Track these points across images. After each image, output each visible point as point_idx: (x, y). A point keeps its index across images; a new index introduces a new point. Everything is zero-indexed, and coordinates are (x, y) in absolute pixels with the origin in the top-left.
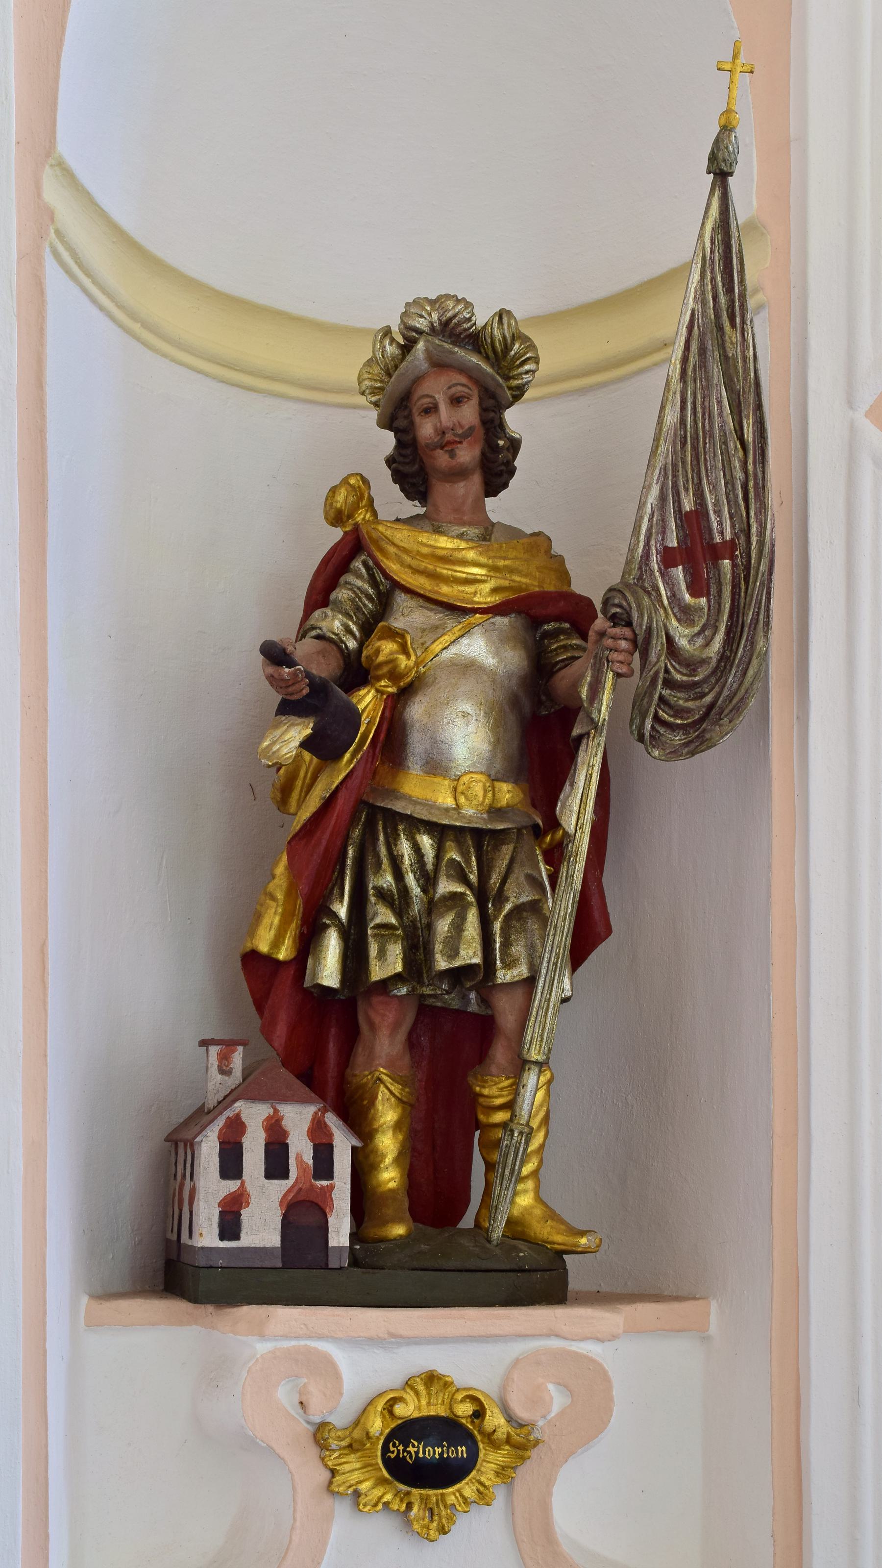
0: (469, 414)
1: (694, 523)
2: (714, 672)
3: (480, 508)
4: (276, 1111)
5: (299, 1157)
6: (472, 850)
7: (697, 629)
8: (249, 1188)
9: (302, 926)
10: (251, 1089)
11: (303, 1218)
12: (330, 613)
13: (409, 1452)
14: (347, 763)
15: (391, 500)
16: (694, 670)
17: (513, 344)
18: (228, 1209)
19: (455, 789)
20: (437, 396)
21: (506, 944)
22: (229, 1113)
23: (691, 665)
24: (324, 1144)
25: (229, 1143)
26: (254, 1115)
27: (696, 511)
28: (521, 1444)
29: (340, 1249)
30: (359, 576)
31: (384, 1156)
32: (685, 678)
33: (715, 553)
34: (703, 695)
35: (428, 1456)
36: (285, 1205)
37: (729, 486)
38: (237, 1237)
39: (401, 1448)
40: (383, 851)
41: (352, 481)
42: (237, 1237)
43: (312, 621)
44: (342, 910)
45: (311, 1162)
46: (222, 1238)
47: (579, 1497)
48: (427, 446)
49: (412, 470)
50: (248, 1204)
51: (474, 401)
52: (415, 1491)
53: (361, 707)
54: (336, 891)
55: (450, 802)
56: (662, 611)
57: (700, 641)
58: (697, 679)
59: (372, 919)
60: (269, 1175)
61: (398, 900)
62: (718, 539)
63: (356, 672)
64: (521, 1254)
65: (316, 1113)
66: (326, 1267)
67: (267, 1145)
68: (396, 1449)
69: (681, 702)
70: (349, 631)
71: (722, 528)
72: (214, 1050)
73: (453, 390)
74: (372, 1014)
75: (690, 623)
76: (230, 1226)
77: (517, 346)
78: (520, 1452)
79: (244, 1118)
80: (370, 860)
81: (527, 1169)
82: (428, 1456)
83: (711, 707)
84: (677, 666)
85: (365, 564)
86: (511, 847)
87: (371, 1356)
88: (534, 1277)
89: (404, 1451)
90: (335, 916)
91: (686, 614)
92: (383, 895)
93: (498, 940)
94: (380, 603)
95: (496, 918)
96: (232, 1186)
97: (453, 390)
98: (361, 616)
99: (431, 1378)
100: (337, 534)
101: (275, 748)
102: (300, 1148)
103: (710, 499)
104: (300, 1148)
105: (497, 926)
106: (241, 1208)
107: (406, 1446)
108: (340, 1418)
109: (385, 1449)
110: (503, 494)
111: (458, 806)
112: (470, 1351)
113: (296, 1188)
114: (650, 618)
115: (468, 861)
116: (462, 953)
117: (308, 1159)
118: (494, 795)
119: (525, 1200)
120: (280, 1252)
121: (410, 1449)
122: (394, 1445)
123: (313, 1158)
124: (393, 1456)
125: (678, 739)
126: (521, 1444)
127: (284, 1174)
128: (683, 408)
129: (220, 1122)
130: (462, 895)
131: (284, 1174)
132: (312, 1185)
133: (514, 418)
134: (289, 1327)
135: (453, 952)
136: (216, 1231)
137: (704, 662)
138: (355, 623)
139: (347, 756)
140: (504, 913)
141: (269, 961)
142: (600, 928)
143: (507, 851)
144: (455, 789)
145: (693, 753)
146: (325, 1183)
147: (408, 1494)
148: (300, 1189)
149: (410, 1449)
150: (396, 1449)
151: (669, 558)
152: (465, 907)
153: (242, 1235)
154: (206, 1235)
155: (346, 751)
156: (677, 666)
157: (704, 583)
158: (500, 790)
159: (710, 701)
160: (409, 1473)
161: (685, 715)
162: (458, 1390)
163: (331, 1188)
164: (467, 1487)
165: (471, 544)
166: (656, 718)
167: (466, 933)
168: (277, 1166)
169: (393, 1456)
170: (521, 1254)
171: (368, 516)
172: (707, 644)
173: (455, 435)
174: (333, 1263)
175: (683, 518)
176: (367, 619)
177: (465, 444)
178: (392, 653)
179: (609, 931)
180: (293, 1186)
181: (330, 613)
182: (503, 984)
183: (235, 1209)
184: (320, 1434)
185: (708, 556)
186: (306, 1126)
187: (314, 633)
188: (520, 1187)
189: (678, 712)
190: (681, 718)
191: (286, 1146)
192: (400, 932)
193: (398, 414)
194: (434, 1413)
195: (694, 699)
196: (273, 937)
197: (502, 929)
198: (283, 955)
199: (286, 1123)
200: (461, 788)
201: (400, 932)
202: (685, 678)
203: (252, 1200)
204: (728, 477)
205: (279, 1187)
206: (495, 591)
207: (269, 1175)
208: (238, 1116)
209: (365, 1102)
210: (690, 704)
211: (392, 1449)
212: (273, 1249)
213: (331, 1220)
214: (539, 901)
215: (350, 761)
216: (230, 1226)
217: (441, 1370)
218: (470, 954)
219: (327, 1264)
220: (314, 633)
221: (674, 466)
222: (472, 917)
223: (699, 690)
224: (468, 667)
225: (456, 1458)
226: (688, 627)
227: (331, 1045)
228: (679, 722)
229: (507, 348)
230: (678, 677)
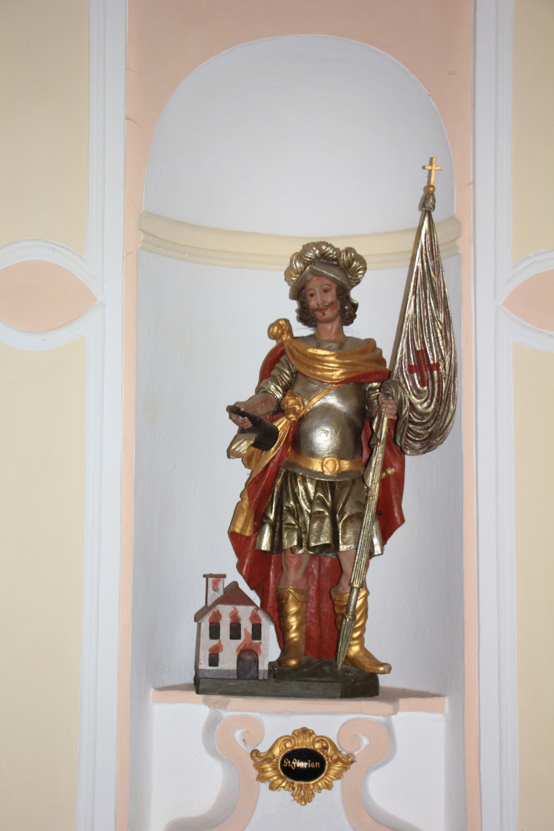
0: (330, 297)
1: (421, 355)
2: (432, 418)
3: (340, 331)
4: (235, 609)
5: (246, 630)
6: (329, 491)
7: (423, 400)
8: (222, 643)
9: (254, 522)
10: (222, 600)
11: (248, 656)
12: (270, 382)
13: (293, 764)
14: (273, 452)
15: (301, 330)
16: (423, 417)
17: (353, 263)
18: (213, 652)
19: (322, 463)
20: (316, 290)
21: (344, 533)
22: (214, 610)
23: (422, 415)
24: (257, 624)
25: (214, 623)
26: (225, 610)
27: (422, 350)
28: (347, 762)
29: (264, 671)
30: (283, 365)
31: (292, 627)
32: (419, 421)
33: (431, 368)
34: (428, 428)
35: (304, 766)
36: (239, 651)
37: (436, 340)
38: (217, 665)
39: (289, 762)
40: (290, 491)
41: (281, 322)
42: (217, 665)
43: (262, 385)
44: (272, 517)
45: (251, 632)
46: (210, 665)
47: (382, 788)
48: (313, 310)
49: (306, 316)
50: (222, 650)
51: (334, 291)
52: (296, 783)
53: (279, 428)
54: (270, 507)
55: (319, 470)
56: (408, 392)
57: (425, 405)
58: (424, 421)
59: (285, 521)
60: (232, 638)
61: (297, 512)
62: (432, 362)
63: (280, 410)
64: (350, 675)
65: (253, 610)
66: (257, 678)
67: (231, 624)
68: (287, 763)
69: (418, 431)
70: (278, 390)
71: (432, 358)
72: (211, 580)
73: (323, 287)
74: (287, 562)
75: (420, 398)
76: (214, 660)
77: (355, 263)
78: (345, 766)
79: (221, 612)
80: (285, 494)
81: (356, 635)
82: (304, 766)
83: (431, 433)
84: (416, 415)
85: (285, 360)
86: (348, 489)
87: (279, 721)
88: (362, 683)
89: (291, 763)
90: (269, 519)
91: (419, 394)
92: (290, 510)
93: (340, 531)
94: (293, 377)
95: (340, 522)
96: (215, 642)
97: (323, 287)
98: (284, 383)
99: (305, 731)
100: (273, 344)
101: (238, 449)
102: (246, 626)
103: (428, 346)
104: (246, 626)
105: (340, 525)
106: (219, 652)
107: (291, 761)
108: (263, 748)
109: (282, 762)
110: (355, 321)
111: (323, 472)
112: (326, 719)
113: (244, 644)
114: (401, 396)
115: (327, 497)
116: (322, 539)
117: (250, 630)
118: (340, 466)
119: (355, 649)
120: (236, 672)
121: (293, 763)
122: (286, 761)
123: (252, 630)
124: (285, 766)
125: (418, 446)
126: (347, 762)
127: (239, 637)
128: (415, 307)
129: (210, 614)
130: (323, 512)
131: (239, 637)
132: (251, 643)
133: (355, 294)
134: (238, 708)
135: (318, 540)
136: (208, 662)
137: (428, 414)
138: (280, 386)
139: (273, 449)
140: (344, 519)
141: (240, 536)
142: (399, 521)
143: (346, 491)
144: (322, 463)
145: (424, 453)
146: (257, 641)
147: (293, 783)
148: (246, 644)
149: (293, 763)
150: (287, 763)
151: (411, 370)
152: (324, 517)
153: (220, 664)
154: (204, 665)
155: (272, 446)
156: (416, 415)
157: (426, 380)
158: (343, 464)
159: (433, 430)
160: (292, 774)
161: (421, 436)
162: (317, 737)
163: (260, 643)
164: (320, 782)
165: (332, 353)
166: (407, 436)
167: (323, 530)
168: (235, 633)
169: (285, 766)
170: (350, 675)
171: (289, 337)
172: (429, 406)
173: (324, 306)
174: (261, 677)
175: (417, 353)
176: (286, 384)
177: (329, 309)
178: (293, 404)
179: (403, 521)
180: (243, 643)
181: (270, 382)
182: (342, 551)
183: (216, 652)
184: (255, 753)
185: (428, 369)
186: (249, 615)
187: (262, 390)
188: (352, 643)
189: (418, 435)
190: (419, 438)
191: (239, 625)
192: (297, 527)
193: (299, 293)
194: (305, 747)
195: (424, 430)
196: (242, 526)
197: (342, 526)
198: (247, 534)
199: (240, 615)
200: (324, 463)
201: (297, 527)
202: (419, 421)
203: (224, 648)
204: (435, 336)
205: (236, 643)
206: (342, 374)
207: (232, 638)
208: (218, 612)
209: (284, 601)
210: (422, 432)
211: (285, 762)
212: (233, 670)
213: (260, 658)
214: (361, 513)
215: (274, 451)
216: (214, 660)
217: (309, 727)
218: (325, 540)
219: (258, 678)
220: (262, 390)
221: (412, 330)
222: (327, 521)
223: (426, 425)
224: (327, 409)
225: (314, 768)
226: (419, 399)
227: (271, 573)
228: (417, 439)
229: (350, 264)
230: (416, 420)
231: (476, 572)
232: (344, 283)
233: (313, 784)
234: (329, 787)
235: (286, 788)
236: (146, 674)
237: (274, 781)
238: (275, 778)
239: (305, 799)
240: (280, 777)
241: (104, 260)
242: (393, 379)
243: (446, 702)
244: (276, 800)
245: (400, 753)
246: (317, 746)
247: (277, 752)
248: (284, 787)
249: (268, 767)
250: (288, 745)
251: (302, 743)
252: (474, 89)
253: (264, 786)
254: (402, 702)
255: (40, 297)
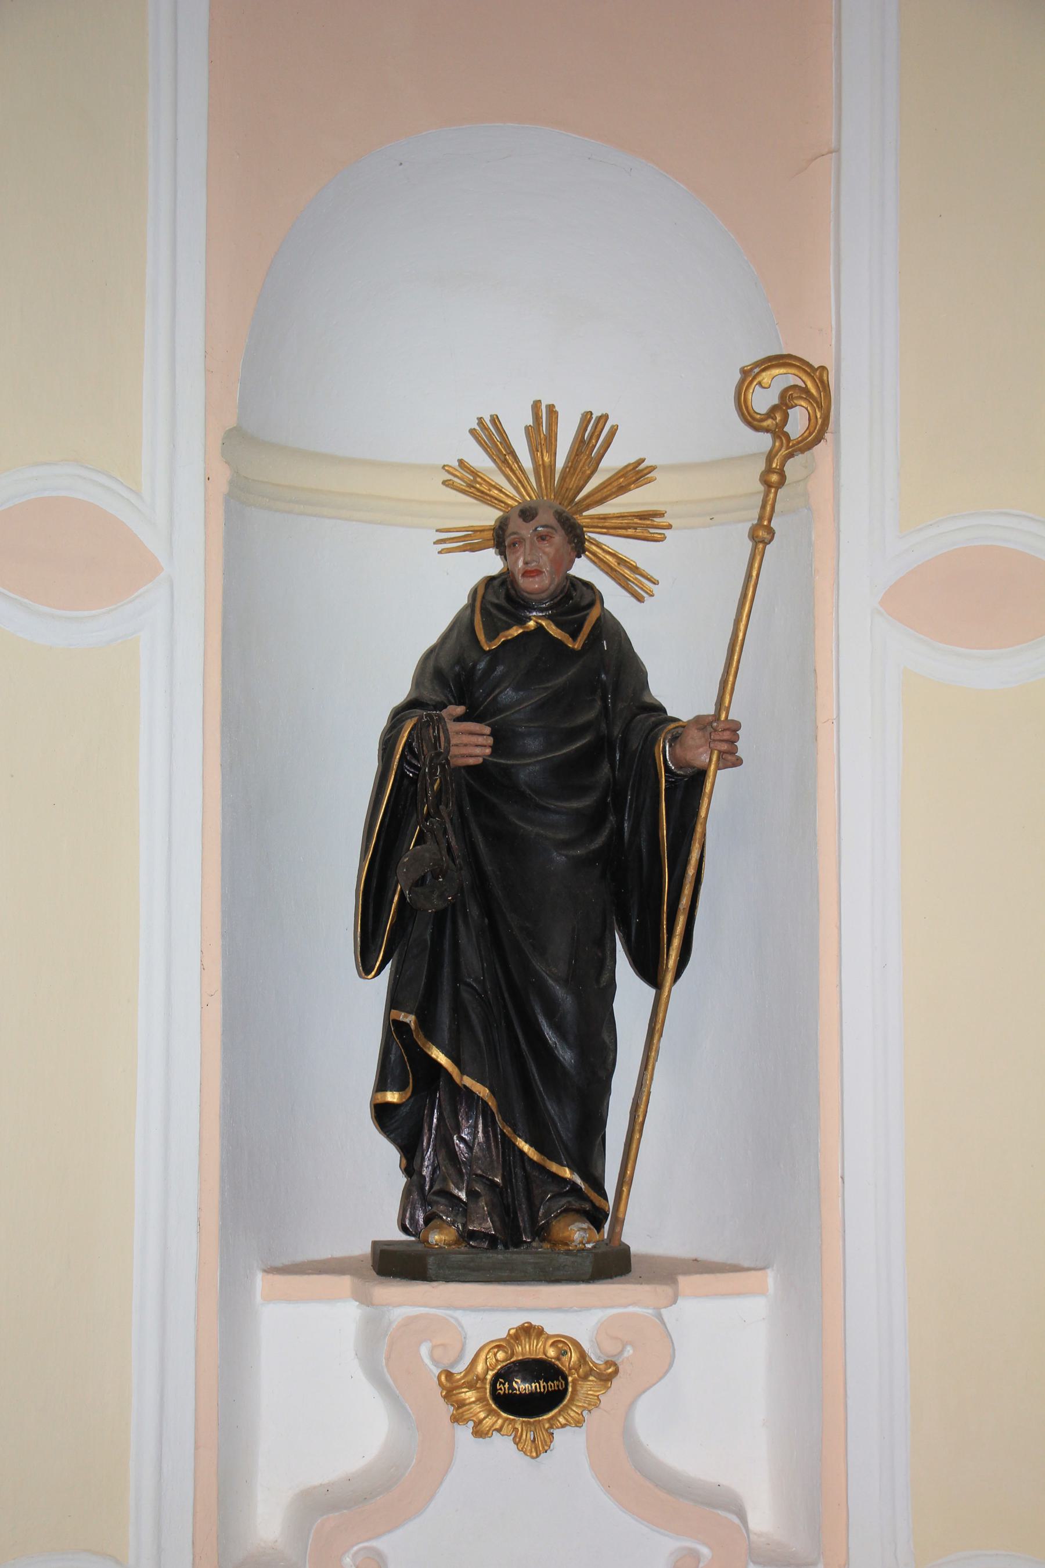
35: (532, 1391)
68: (503, 1388)
87: (480, 1319)
99: (528, 1331)
126: (607, 1375)
134: (408, 1301)
231: (841, 1243)
232: (438, 699)
233: (549, 1420)
234: (579, 1423)
235: (504, 1431)
236: (252, 1216)
237: (481, 1421)
238: (482, 1415)
239: (538, 1448)
240: (490, 1412)
241: (167, 496)
242: (577, 646)
243: (770, 1278)
244: (490, 1456)
245: (699, 1372)
246: (552, 1353)
247: (480, 1368)
248: (499, 1430)
249: (470, 1396)
250: (501, 1355)
251: (527, 1350)
252: (196, 1419)
253: (464, 1432)
254: (683, 1281)
255: (73, 556)
